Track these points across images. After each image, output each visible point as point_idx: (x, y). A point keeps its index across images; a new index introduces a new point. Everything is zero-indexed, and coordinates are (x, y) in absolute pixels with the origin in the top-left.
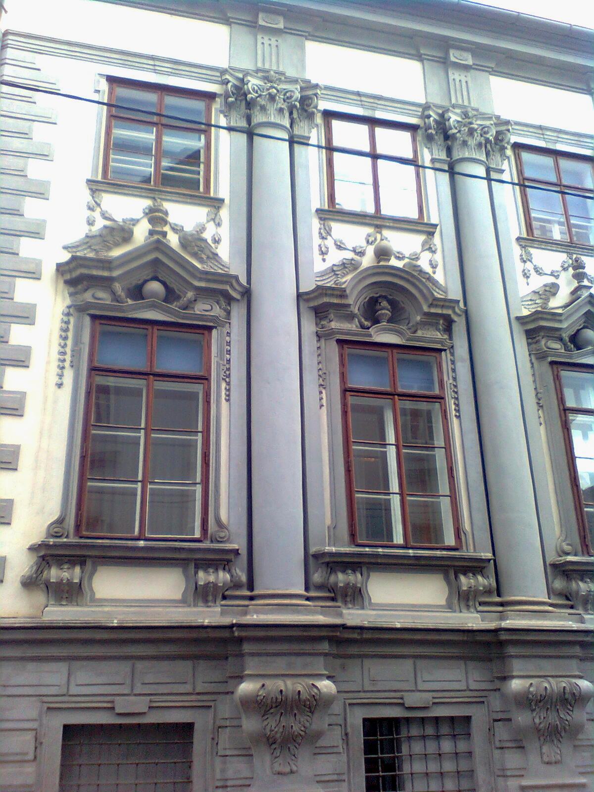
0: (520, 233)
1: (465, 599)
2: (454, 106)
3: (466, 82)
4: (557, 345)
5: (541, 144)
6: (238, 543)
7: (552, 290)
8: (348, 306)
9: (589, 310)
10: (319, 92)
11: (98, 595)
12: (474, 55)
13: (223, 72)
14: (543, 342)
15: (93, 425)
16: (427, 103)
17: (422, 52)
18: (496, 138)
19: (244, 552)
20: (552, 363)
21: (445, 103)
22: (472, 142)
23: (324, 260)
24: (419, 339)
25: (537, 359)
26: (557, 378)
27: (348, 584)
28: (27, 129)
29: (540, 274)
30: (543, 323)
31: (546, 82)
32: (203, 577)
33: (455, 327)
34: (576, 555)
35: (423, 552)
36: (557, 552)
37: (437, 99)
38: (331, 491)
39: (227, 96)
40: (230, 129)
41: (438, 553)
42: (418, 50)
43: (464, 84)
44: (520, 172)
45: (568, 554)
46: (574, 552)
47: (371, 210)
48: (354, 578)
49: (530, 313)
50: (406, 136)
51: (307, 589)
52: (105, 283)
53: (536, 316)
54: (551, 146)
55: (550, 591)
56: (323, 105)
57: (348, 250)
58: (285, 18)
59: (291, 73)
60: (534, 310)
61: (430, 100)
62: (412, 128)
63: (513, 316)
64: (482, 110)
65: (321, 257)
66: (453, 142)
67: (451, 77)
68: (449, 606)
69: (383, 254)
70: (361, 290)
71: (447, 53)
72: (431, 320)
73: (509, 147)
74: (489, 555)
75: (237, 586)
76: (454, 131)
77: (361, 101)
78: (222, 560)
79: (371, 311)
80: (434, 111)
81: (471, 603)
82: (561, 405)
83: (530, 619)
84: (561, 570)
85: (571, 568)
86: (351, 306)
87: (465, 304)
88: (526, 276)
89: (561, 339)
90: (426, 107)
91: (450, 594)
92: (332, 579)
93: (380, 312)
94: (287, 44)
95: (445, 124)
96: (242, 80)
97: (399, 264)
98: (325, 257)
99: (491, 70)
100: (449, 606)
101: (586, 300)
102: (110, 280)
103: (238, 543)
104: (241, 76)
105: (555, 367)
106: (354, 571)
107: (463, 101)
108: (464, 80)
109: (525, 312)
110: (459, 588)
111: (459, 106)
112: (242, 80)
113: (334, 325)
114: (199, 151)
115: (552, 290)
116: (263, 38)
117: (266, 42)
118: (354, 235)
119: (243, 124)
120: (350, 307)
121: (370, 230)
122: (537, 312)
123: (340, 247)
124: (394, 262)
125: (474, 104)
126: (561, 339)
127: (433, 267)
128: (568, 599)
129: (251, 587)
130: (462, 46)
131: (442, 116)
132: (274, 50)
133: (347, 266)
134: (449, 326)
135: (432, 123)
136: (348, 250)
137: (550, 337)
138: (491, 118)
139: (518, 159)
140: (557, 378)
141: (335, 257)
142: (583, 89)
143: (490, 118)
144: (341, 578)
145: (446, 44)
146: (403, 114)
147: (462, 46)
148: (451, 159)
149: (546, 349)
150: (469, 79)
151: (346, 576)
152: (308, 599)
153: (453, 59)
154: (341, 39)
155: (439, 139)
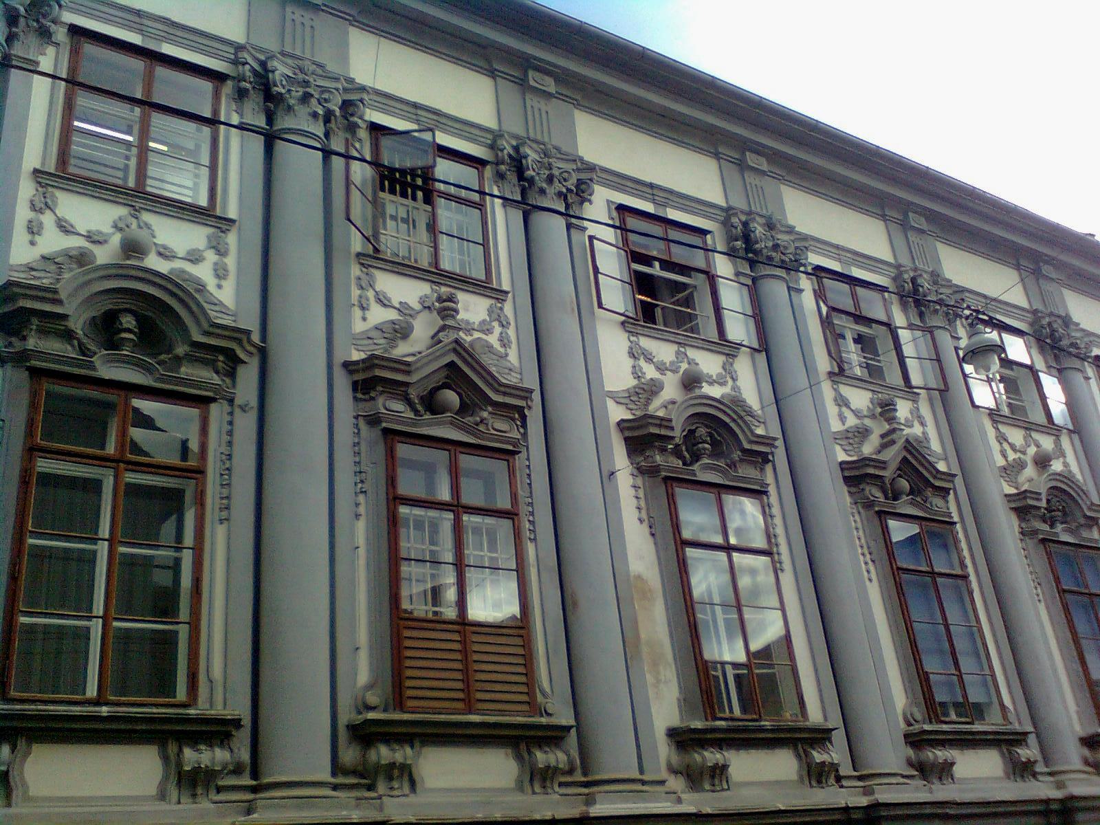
0: (43, 164)
1: (542, 777)
2: (283, 54)
3: (532, 107)
4: (398, 406)
5: (135, 38)
6: (240, 708)
7: (401, 331)
8: (64, 317)
9: (453, 361)
10: (365, 96)
11: (32, 792)
12: (558, 80)
13: (239, 48)
14: (380, 401)
15: (30, 532)
16: (500, 131)
17: (720, 150)
18: (577, 186)
19: (247, 721)
20: (666, 479)
21: (522, 133)
22: (551, 191)
23: (32, 243)
24: (182, 381)
25: (863, 507)
26: (391, 454)
27: (717, 764)
28: (390, 210)
29: (385, 305)
30: (378, 372)
31: (389, 33)
32: (190, 757)
33: (241, 371)
34: (385, 710)
35: (52, 708)
36: (357, 707)
37: (515, 126)
38: (884, 669)
39: (498, 163)
40: (241, 127)
41: (76, 710)
42: (489, 62)
43: (544, 115)
44: (73, 69)
45: (373, 708)
46: (383, 706)
47: (203, 202)
48: (401, 754)
49: (366, 356)
50: (207, 86)
51: (334, 774)
52: (398, 389)
53: (371, 362)
54: (152, 45)
55: (337, 768)
56: (815, 259)
57: (79, 234)
58: (767, 160)
59: (332, 67)
60: (370, 353)
61: (732, 203)
62: (217, 77)
63: (339, 357)
64: (564, 149)
65: (29, 237)
66: (276, 106)
67: (289, 16)
68: (520, 787)
69: (132, 248)
70: (96, 294)
71: (526, 75)
72: (204, 353)
73: (363, 125)
74: (572, 722)
75: (237, 770)
76: (533, 173)
77: (653, 195)
78: (553, 736)
79: (106, 327)
80: (507, 142)
81: (548, 784)
82: (391, 490)
83: (627, 801)
84: (916, 740)
85: (373, 729)
86: (70, 319)
87: (264, 338)
88: (34, 229)
89: (68, 335)
90: (497, 135)
91: (165, 778)
92: (372, 756)
93: (700, 445)
94: (555, 108)
95: (268, 78)
96: (263, 64)
97: (163, 266)
98: (37, 238)
99: (351, 18)
100: (520, 787)
101: (451, 347)
102: (407, 384)
103: (565, 717)
104: (262, 58)
105: (669, 483)
106: (222, 745)
107: (543, 137)
108: (544, 108)
109: (356, 356)
110: (179, 764)
111: (293, 56)
112: (263, 64)
113: (32, 343)
114: (636, 272)
115: (401, 331)
116: (293, 13)
117: (297, 17)
118: (92, 216)
119: (261, 122)
120: (68, 320)
121: (122, 211)
122: (373, 357)
123: (65, 228)
124: (153, 262)
125: (555, 142)
126: (68, 335)
127: (218, 276)
128: (362, 776)
129: (255, 774)
130: (759, 150)
131: (516, 149)
132: (308, 29)
133: (81, 259)
134: (234, 361)
135: (248, 74)
136: (79, 234)
137: (394, 396)
138: (575, 161)
139: (75, 52)
140: (391, 454)
141: (52, 242)
142: (710, 153)
143: (337, 79)
144: (384, 754)
145: (526, 63)
146: (202, 52)
147: (759, 150)
148: (271, 127)
149: (872, 498)
150: (316, 23)
151: (391, 753)
152: (335, 787)
153: (532, 83)
154: (420, 42)
155: (512, 177)
